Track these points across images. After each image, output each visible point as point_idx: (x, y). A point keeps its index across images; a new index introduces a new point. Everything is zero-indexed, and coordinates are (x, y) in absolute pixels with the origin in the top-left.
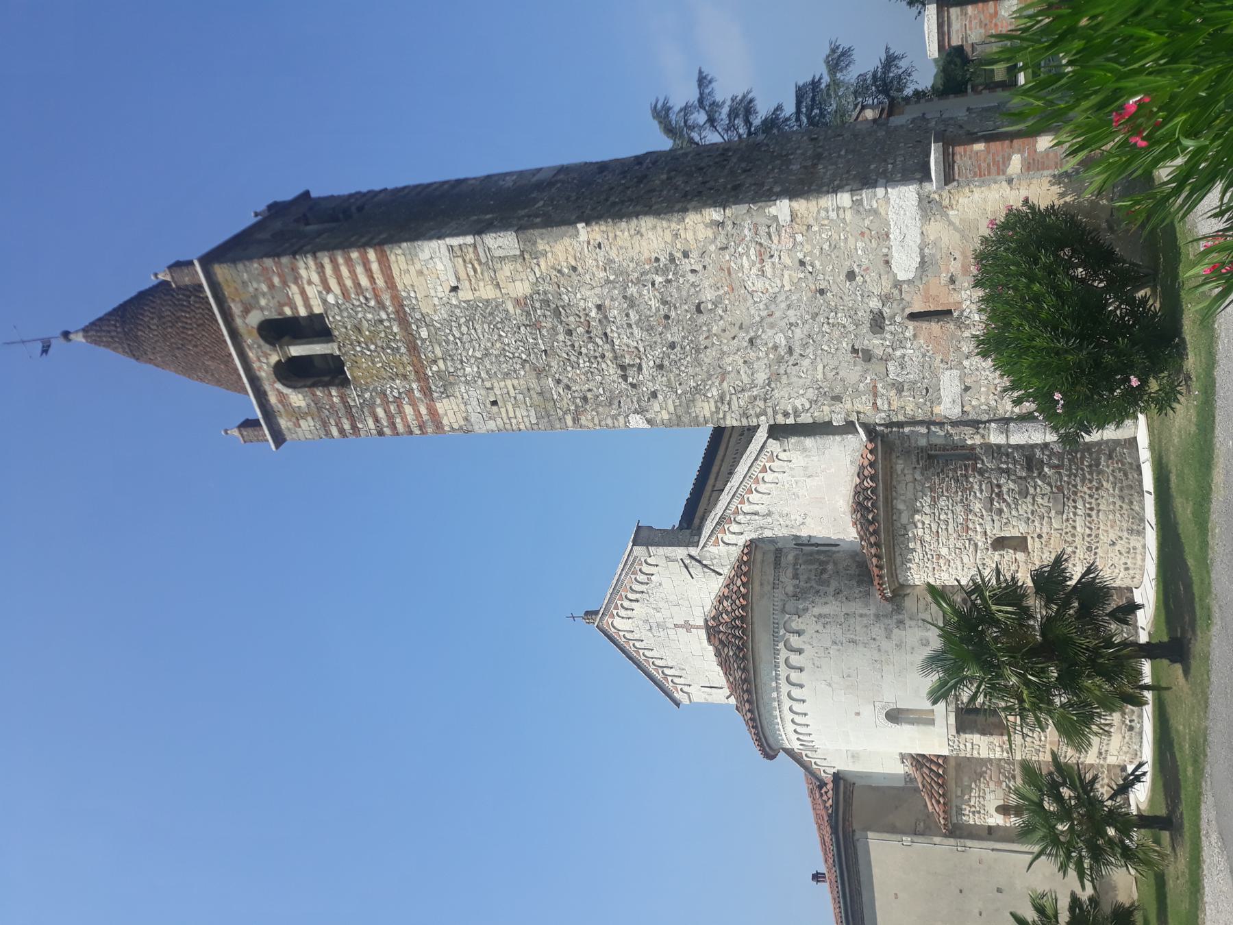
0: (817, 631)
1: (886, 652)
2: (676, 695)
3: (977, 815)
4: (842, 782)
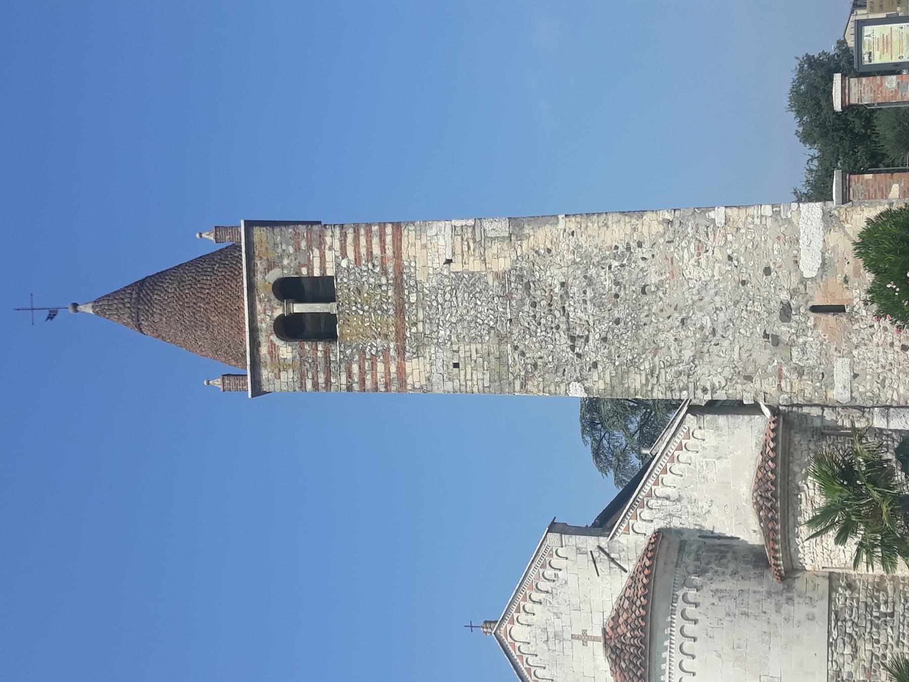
0: (713, 604)
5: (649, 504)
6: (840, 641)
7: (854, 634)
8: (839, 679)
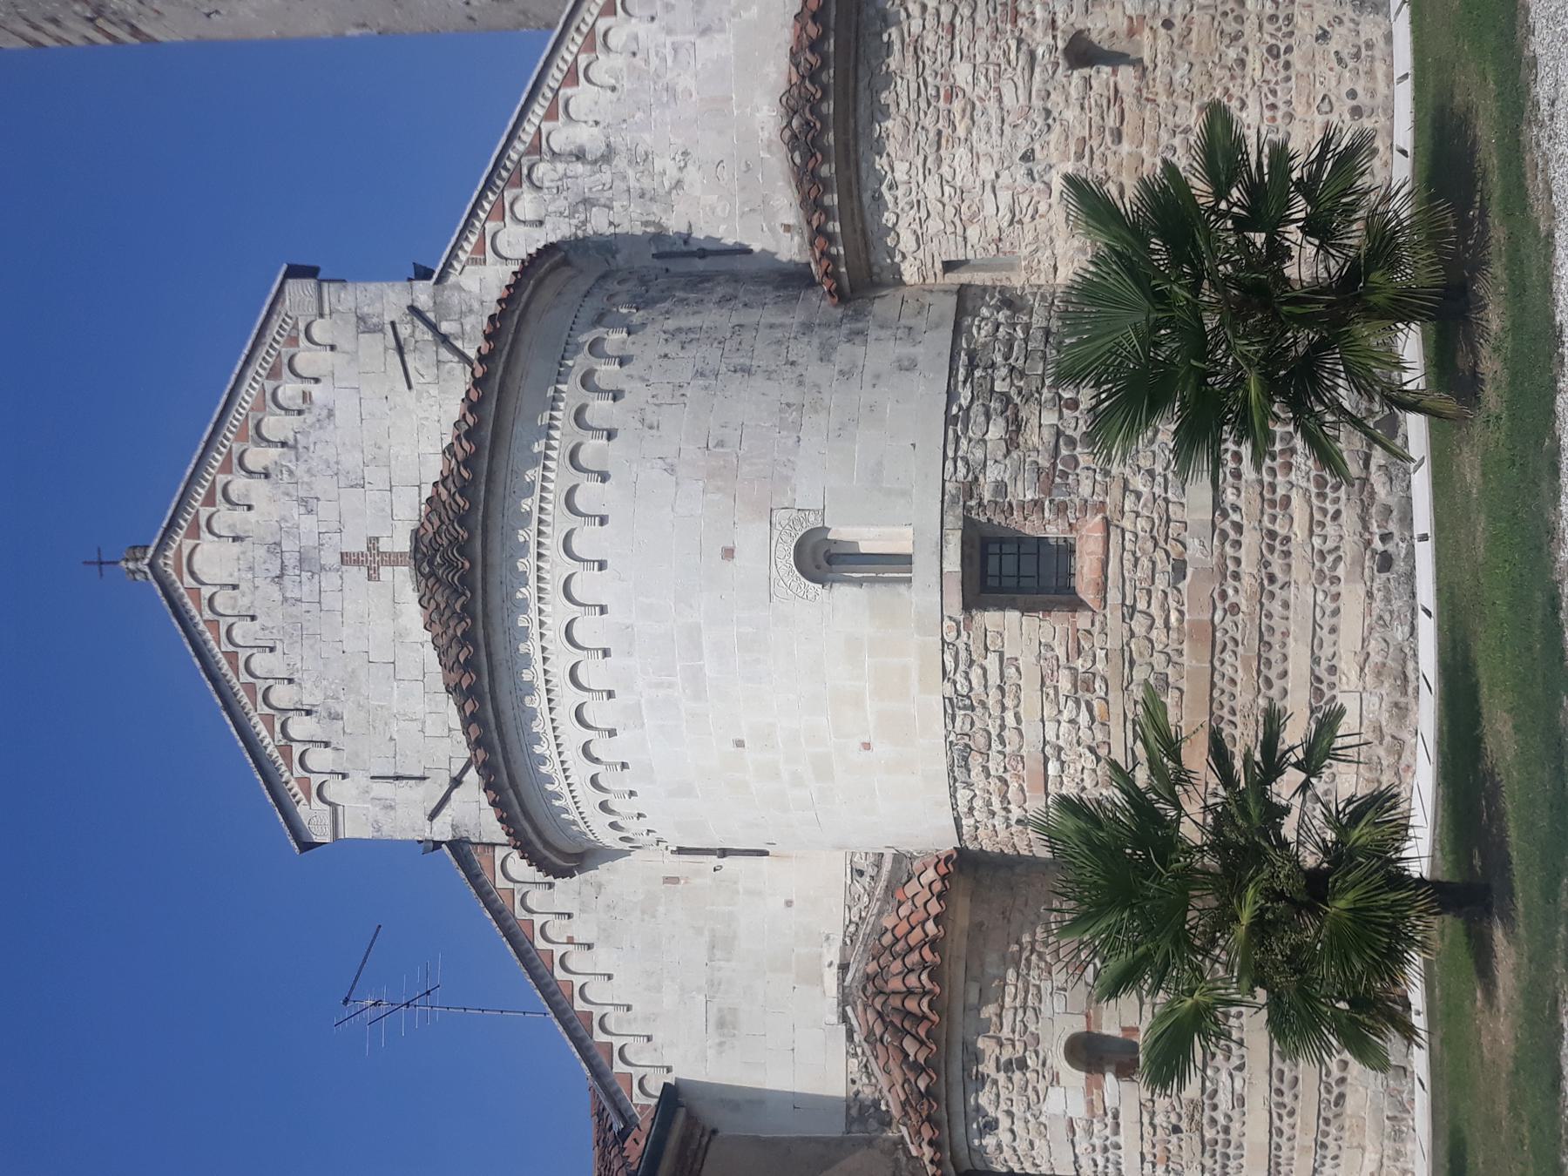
0: (666, 356)
1: (816, 385)
2: (303, 811)
3: (1017, 1075)
5: (534, 176)
6: (977, 408)
7: (1013, 393)
8: (973, 503)
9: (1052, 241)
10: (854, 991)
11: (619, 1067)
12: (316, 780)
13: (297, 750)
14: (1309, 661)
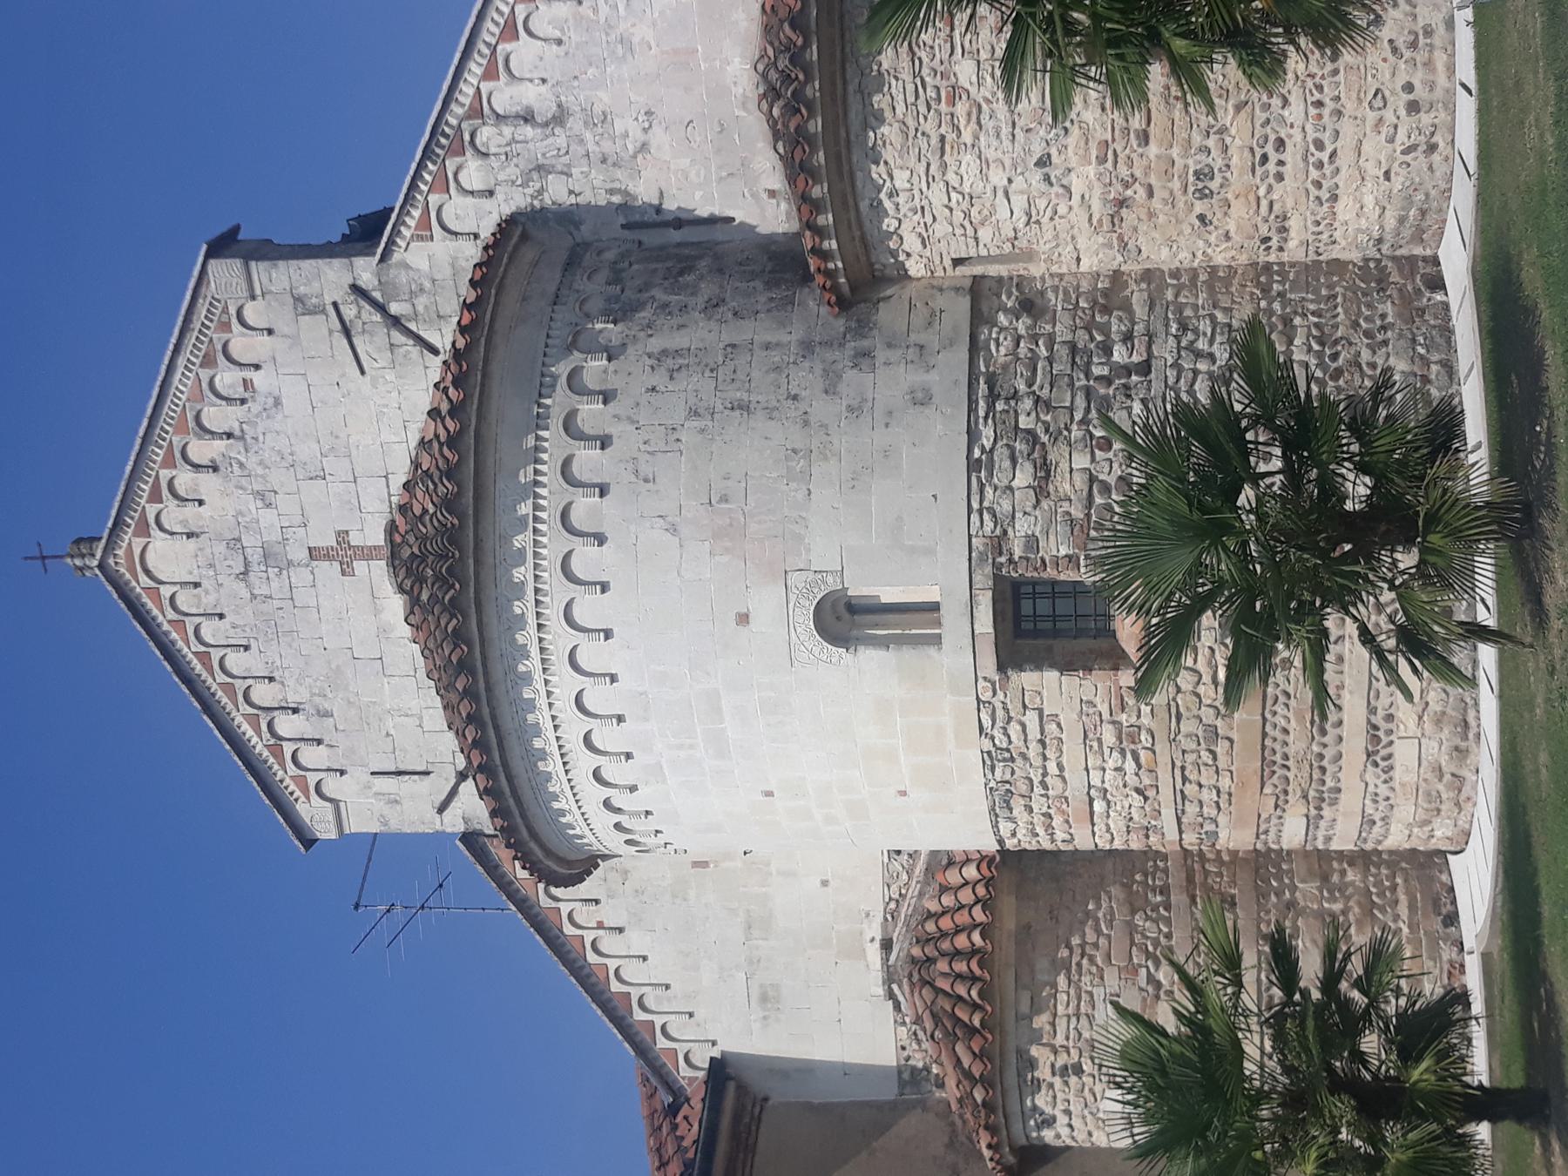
0: (653, 389)
2: (302, 809)
3: (1073, 1080)
4: (731, 1086)
5: (478, 141)
6: (1001, 454)
7: (1040, 431)
8: (1003, 559)
9: (1073, 238)
10: (899, 969)
11: (662, 1043)
12: (312, 778)
13: (288, 749)
14: (1364, 711)
